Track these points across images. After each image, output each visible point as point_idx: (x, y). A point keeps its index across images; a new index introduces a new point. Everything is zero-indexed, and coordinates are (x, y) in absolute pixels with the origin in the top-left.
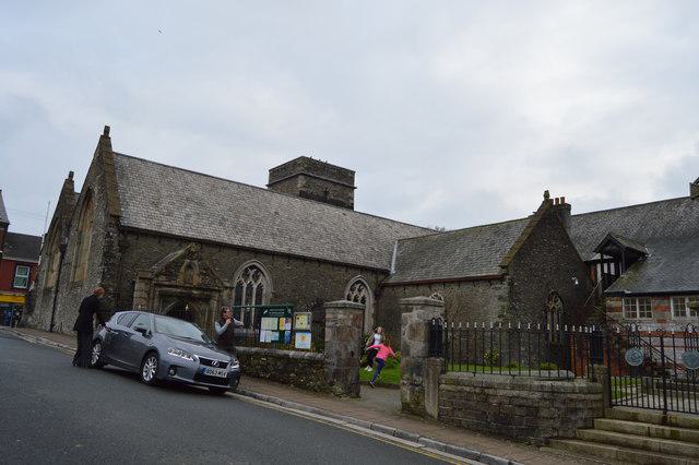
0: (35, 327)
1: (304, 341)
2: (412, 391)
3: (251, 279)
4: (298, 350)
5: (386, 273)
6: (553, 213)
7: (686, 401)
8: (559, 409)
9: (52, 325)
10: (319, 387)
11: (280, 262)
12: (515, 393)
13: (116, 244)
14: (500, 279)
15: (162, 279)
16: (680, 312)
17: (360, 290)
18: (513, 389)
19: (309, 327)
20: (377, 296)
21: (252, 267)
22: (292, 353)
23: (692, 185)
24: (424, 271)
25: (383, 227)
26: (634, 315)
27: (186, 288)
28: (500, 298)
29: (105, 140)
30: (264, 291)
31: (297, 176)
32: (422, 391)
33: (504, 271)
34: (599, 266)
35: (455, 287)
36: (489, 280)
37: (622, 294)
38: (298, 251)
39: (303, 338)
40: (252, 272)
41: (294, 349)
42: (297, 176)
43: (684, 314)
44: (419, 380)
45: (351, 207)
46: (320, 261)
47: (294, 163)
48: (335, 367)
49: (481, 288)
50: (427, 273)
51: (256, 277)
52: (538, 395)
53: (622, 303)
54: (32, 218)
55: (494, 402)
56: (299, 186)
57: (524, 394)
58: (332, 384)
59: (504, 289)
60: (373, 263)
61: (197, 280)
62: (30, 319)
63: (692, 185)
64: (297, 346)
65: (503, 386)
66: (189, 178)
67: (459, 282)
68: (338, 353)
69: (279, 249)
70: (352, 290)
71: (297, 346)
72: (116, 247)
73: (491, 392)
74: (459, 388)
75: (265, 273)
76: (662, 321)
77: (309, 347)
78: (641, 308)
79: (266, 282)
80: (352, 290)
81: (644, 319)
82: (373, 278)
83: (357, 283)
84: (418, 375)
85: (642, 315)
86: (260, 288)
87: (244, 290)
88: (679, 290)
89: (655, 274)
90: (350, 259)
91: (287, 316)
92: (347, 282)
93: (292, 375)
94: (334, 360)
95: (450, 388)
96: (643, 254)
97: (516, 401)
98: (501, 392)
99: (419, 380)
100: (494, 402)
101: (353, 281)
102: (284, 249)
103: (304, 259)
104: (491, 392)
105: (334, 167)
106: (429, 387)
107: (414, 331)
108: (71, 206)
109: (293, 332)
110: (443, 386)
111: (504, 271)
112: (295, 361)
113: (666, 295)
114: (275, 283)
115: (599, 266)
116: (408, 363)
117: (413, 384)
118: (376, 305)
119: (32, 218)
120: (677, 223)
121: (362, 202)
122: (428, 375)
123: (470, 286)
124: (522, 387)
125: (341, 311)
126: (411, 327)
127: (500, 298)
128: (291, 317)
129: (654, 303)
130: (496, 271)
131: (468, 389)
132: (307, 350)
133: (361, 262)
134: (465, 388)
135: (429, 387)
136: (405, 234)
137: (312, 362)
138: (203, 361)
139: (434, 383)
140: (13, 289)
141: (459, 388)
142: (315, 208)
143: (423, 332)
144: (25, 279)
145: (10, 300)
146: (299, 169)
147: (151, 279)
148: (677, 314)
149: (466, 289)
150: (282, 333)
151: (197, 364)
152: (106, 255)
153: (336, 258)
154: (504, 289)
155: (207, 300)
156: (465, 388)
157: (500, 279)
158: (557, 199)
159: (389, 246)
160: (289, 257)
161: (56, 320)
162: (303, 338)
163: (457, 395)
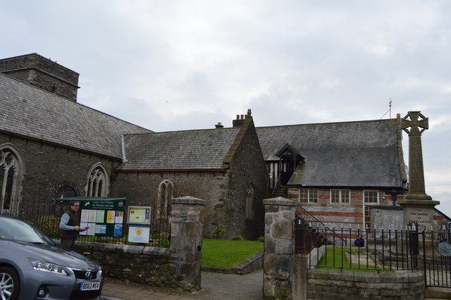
1: (140, 235)
2: (278, 285)
3: (95, 176)
4: (132, 244)
5: (120, 161)
6: (244, 123)
7: (432, 272)
8: (411, 295)
10: (163, 282)
11: (34, 146)
12: (383, 285)
14: (222, 172)
16: (335, 200)
17: (98, 175)
18: (382, 282)
19: (148, 222)
20: (112, 180)
21: (6, 150)
22: (126, 248)
24: (154, 161)
25: (111, 123)
26: (306, 201)
28: (222, 186)
30: (16, 174)
31: (28, 69)
32: (289, 285)
33: (226, 166)
34: (272, 165)
35: (184, 177)
36: (213, 172)
37: (300, 186)
38: (49, 138)
39: (139, 233)
40: (5, 155)
41: (126, 242)
42: (28, 69)
43: (338, 201)
44: (286, 275)
45: (73, 97)
46: (69, 148)
47: (25, 58)
48: (184, 262)
49: (206, 178)
50: (158, 164)
51: (8, 160)
52: (399, 286)
53: (298, 192)
55: (365, 294)
56: (30, 79)
57: (390, 285)
58: (179, 279)
59: (225, 179)
60: (109, 152)
64: (130, 240)
65: (373, 280)
67: (188, 172)
68: (187, 248)
69: (32, 135)
70: (93, 174)
71: (130, 240)
73: (362, 285)
74: (329, 282)
75: (19, 157)
76: (324, 205)
77: (147, 241)
78: (311, 196)
79: (18, 165)
80: (93, 174)
81: (344, 204)
82: (109, 165)
83: (97, 168)
84: (286, 270)
85: (311, 200)
86: (12, 171)
87: (6, 172)
88: (336, 185)
89: (307, 175)
90: (92, 148)
91: (116, 208)
92: (90, 167)
93: (127, 270)
94: (183, 255)
95: (318, 282)
96: (303, 159)
97: (385, 293)
98: (372, 285)
99: (286, 275)
100: (365, 294)
101: (95, 166)
102: (37, 135)
103: (55, 146)
104: (362, 285)
105: (62, 67)
106: (297, 281)
107: (280, 230)
108: (237, 123)
109: (126, 226)
110: (311, 281)
111: (226, 166)
112: (131, 256)
113: (327, 188)
114: (27, 166)
115: (272, 165)
116: (273, 259)
117: (279, 279)
118: (111, 187)
120: (315, 140)
121: (83, 96)
122: (295, 271)
123: (198, 176)
124: (389, 280)
125: (191, 208)
126: (276, 226)
127: (222, 186)
128: (123, 209)
129: (319, 193)
130: (218, 166)
131: (338, 283)
132: (144, 245)
133: (101, 151)
134: (335, 282)
135: (297, 281)
136: (127, 130)
137: (153, 257)
138: (80, 274)
139: (302, 277)
141: (329, 282)
142: (42, 96)
143: (289, 231)
146: (31, 64)
148: (333, 201)
149: (192, 177)
150: (110, 227)
151: (73, 277)
153: (81, 146)
154: (225, 179)
156: (335, 282)
157: (222, 172)
158: (242, 116)
159: (118, 139)
160: (42, 142)
162: (139, 233)
163: (327, 288)
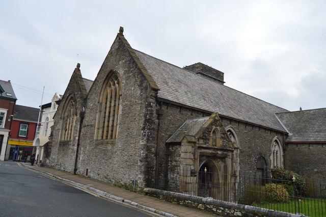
0: (52, 167)
9: (75, 170)
13: (155, 112)
15: (201, 141)
23: (223, 73)
27: (214, 149)
29: (120, 37)
54: (40, 87)
61: (220, 143)
62: (48, 161)
63: (223, 73)
66: (171, 68)
72: (155, 115)
75: (236, 136)
118: (284, 156)
119: (40, 87)
140: (18, 137)
144: (25, 131)
145: (16, 143)
147: (195, 143)
152: (147, 121)
155: (223, 158)
161: (79, 165)
